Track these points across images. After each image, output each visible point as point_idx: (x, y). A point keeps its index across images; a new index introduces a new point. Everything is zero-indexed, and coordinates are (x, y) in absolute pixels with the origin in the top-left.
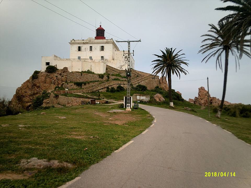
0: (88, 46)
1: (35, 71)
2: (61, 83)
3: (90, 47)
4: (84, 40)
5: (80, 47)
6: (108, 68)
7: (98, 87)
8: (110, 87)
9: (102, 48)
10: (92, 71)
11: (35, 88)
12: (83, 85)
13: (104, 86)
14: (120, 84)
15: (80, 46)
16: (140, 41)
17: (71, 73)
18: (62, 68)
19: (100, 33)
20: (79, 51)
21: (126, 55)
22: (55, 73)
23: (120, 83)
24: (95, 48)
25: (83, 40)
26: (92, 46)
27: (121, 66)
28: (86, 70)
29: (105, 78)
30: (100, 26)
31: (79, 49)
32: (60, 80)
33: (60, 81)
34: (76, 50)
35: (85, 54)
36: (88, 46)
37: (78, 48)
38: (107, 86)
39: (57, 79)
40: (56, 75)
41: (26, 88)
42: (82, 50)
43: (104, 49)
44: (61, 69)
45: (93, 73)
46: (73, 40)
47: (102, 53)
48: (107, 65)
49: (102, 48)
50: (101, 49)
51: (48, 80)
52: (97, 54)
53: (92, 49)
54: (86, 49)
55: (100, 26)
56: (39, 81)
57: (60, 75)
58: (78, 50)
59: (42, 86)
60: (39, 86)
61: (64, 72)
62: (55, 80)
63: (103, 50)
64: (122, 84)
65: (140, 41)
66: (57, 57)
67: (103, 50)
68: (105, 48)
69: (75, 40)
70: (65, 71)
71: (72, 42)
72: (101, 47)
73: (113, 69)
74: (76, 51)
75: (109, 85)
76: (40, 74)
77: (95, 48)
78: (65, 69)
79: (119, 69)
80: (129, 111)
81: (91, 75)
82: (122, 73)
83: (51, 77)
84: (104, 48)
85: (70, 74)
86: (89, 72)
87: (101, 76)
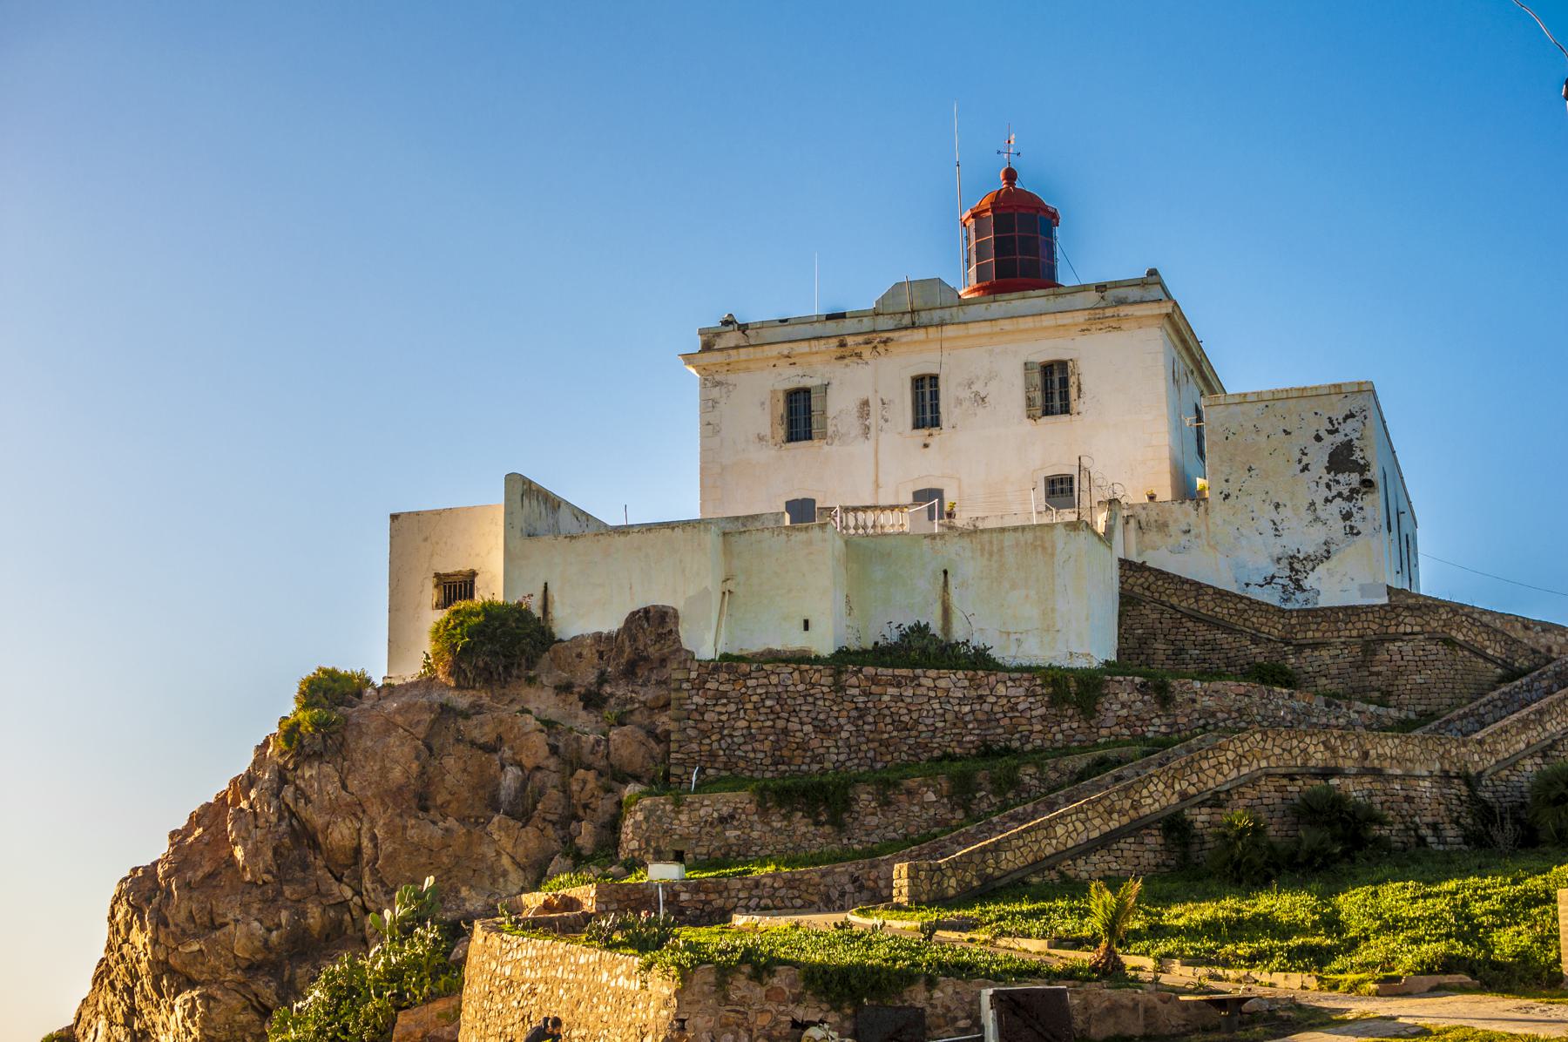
0: (887, 377)
1: (309, 671)
2: (605, 805)
3: (918, 382)
4: (842, 316)
5: (807, 391)
6: (1140, 589)
7: (1049, 825)
8: (1201, 817)
9: (1053, 390)
10: (959, 633)
11: (305, 867)
12: (865, 797)
13: (1122, 812)
14: (1326, 773)
15: (807, 382)
16: (945, 572)
17: (716, 669)
18: (611, 623)
19: (1018, 243)
20: (792, 437)
21: (1339, 438)
22: (531, 681)
23: (1319, 757)
24: (966, 394)
25: (830, 317)
26: (934, 379)
27: (1296, 567)
28: (881, 627)
29: (1123, 698)
30: (1010, 175)
31: (800, 417)
32: (588, 768)
33: (591, 775)
34: (767, 431)
35: (869, 469)
36: (887, 377)
37: (781, 408)
38: (1156, 797)
39: (554, 750)
40: (543, 701)
41: (210, 876)
42: (830, 430)
43: (1073, 392)
44: (598, 637)
45: (981, 661)
46: (726, 323)
47: (1055, 445)
48: (1125, 564)
49: (1053, 390)
50: (1038, 396)
51: (454, 769)
52: (993, 462)
53: (935, 409)
54: (875, 407)
55: (1010, 175)
56: (354, 783)
57: (592, 701)
58: (781, 432)
59: (387, 847)
60: (358, 850)
61: (630, 672)
62: (529, 763)
63: (1066, 409)
64: (1349, 765)
65: (945, 572)
66: (551, 503)
67: (1066, 409)
68: (839, 407)
69: (743, 328)
70: (646, 659)
71: (720, 343)
72: (1037, 379)
73: (1206, 606)
74: (761, 438)
75: (1184, 796)
76: (367, 705)
77: (966, 394)
78: (654, 623)
79: (1271, 597)
80: (860, 787)
81: (953, 682)
82: (1315, 646)
83: (481, 730)
84: (1072, 380)
85: (700, 685)
86: (921, 650)
87: (1072, 690)
